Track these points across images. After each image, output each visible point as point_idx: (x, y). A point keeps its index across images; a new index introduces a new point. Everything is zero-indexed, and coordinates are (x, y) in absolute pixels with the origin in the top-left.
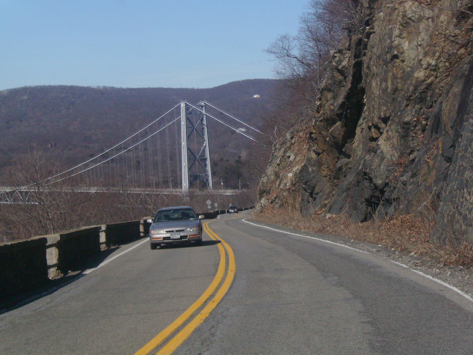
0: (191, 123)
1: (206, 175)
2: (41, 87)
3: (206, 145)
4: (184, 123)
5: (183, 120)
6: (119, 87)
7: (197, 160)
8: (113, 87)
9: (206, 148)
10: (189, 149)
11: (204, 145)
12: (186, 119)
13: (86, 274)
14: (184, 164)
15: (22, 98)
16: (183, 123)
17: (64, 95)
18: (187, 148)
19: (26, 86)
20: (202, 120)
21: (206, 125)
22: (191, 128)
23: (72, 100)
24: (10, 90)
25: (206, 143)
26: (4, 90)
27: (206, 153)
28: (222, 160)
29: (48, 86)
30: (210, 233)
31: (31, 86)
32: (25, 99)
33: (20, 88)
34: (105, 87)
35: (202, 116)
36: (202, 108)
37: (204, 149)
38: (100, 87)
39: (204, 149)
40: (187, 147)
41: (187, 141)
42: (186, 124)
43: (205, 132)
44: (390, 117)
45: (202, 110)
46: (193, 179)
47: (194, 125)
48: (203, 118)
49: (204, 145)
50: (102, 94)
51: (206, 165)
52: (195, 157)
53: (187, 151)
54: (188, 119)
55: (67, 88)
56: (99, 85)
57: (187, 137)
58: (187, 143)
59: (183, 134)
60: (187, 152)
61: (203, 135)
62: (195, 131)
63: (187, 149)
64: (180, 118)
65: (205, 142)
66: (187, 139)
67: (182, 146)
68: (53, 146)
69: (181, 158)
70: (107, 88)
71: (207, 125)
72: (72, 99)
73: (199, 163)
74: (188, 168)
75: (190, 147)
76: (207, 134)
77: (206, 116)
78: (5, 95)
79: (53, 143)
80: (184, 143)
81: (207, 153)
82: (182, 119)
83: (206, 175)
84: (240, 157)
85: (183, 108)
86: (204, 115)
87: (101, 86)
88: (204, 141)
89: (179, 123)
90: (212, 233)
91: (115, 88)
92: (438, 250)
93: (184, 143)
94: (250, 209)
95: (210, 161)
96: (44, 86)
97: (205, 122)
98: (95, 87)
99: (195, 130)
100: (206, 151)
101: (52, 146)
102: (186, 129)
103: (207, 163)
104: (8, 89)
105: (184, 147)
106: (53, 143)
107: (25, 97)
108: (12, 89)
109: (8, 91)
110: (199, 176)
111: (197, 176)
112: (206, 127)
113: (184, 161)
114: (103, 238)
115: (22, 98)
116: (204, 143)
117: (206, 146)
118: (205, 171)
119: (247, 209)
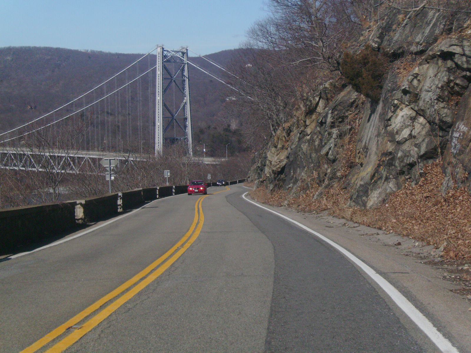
0: (169, 73)
1: (185, 139)
2: (26, 48)
3: (186, 101)
5: (159, 69)
6: (107, 52)
7: (175, 119)
8: (101, 52)
9: (186, 105)
10: (164, 105)
11: (185, 101)
12: (162, 68)
13: (10, 259)
14: (159, 124)
16: (159, 73)
17: (49, 57)
20: (183, 70)
21: (187, 77)
22: (170, 79)
25: (187, 99)
27: (186, 112)
28: (209, 127)
29: (33, 47)
32: (9, 59)
33: (4, 48)
34: (93, 51)
35: (183, 65)
36: (184, 55)
37: (184, 106)
38: (88, 51)
39: (184, 106)
40: (163, 103)
41: (163, 96)
42: (162, 74)
43: (186, 86)
44: (371, 106)
45: (184, 58)
46: (169, 141)
47: (173, 76)
48: (184, 68)
49: (185, 101)
50: (89, 58)
51: (185, 127)
53: (163, 108)
54: (164, 68)
55: (53, 50)
56: (87, 49)
57: (163, 89)
58: (163, 97)
59: (159, 87)
60: (163, 109)
61: (184, 89)
62: (173, 84)
63: (163, 106)
64: (156, 67)
65: (185, 98)
66: (163, 93)
67: (157, 101)
68: (32, 109)
69: (155, 115)
70: (95, 53)
71: (188, 77)
72: (58, 61)
73: (178, 124)
74: (163, 129)
75: (168, 104)
76: (188, 88)
77: (188, 65)
79: (33, 106)
80: (159, 98)
81: (187, 113)
82: (157, 68)
83: (185, 139)
84: (229, 126)
85: (159, 54)
86: (186, 64)
87: (89, 51)
88: (184, 95)
89: (154, 71)
91: (103, 52)
93: (159, 98)
94: (239, 183)
95: (191, 122)
96: (29, 47)
97: (186, 73)
98: (83, 51)
99: (174, 83)
100: (186, 109)
101: (31, 108)
102: (163, 80)
103: (187, 123)
105: (159, 102)
106: (33, 106)
107: (9, 58)
110: (177, 139)
111: (174, 139)
112: (187, 79)
113: (159, 120)
114: (120, 202)
116: (184, 99)
117: (186, 103)
118: (185, 134)
119: (235, 183)
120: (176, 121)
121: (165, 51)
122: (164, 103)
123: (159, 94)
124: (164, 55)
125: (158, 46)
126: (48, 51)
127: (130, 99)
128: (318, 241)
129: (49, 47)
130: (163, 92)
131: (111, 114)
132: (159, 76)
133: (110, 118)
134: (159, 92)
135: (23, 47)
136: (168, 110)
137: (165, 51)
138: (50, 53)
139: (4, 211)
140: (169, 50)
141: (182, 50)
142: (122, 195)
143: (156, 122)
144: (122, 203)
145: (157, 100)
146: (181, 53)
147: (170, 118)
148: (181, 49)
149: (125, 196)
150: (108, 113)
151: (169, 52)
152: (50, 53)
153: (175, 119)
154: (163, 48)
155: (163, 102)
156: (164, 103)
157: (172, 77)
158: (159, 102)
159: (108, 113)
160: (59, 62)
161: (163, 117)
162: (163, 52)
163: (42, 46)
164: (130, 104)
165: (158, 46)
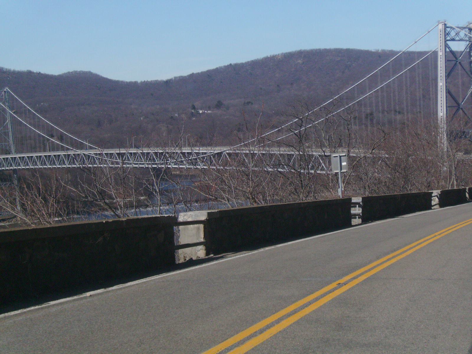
2: (316, 50)
4: (442, 53)
7: (462, 109)
10: (448, 92)
15: (297, 62)
18: (446, 91)
19: (301, 50)
23: (348, 63)
24: (284, 54)
26: (279, 55)
29: (323, 50)
30: (467, 222)
31: (306, 50)
33: (295, 51)
34: (384, 50)
38: (378, 51)
40: (446, 90)
50: (380, 57)
52: (459, 105)
63: (446, 93)
66: (446, 78)
75: (452, 91)
78: (280, 59)
80: (441, 84)
85: (441, 31)
87: (380, 50)
90: (461, 223)
91: (394, 51)
92: (302, 187)
93: (441, 84)
96: (320, 50)
102: (446, 62)
104: (282, 53)
107: (300, 61)
108: (286, 53)
109: (283, 55)
115: (297, 62)
120: (463, 111)
121: (448, 27)
122: (448, 90)
123: (441, 79)
124: (447, 32)
125: (439, 22)
126: (339, 52)
127: (422, 97)
128: (447, 113)
129: (339, 49)
130: (446, 76)
131: (399, 113)
132: (441, 58)
133: (399, 117)
134: (441, 76)
135: (314, 49)
136: (454, 98)
137: (448, 27)
138: (340, 55)
139: (62, 225)
140: (454, 27)
141: (469, 26)
142: (362, 201)
143: (439, 112)
144: (362, 213)
145: (439, 86)
146: (467, 29)
147: (456, 106)
148: (467, 24)
149: (367, 203)
150: (395, 111)
151: (454, 29)
152: (340, 55)
153: (462, 109)
154: (445, 25)
155: (446, 88)
156: (448, 90)
157: (456, 58)
158: (441, 89)
159: (395, 111)
160: (349, 63)
161: (447, 107)
162: (445, 29)
163: (332, 48)
164: (422, 102)
165: (439, 22)
